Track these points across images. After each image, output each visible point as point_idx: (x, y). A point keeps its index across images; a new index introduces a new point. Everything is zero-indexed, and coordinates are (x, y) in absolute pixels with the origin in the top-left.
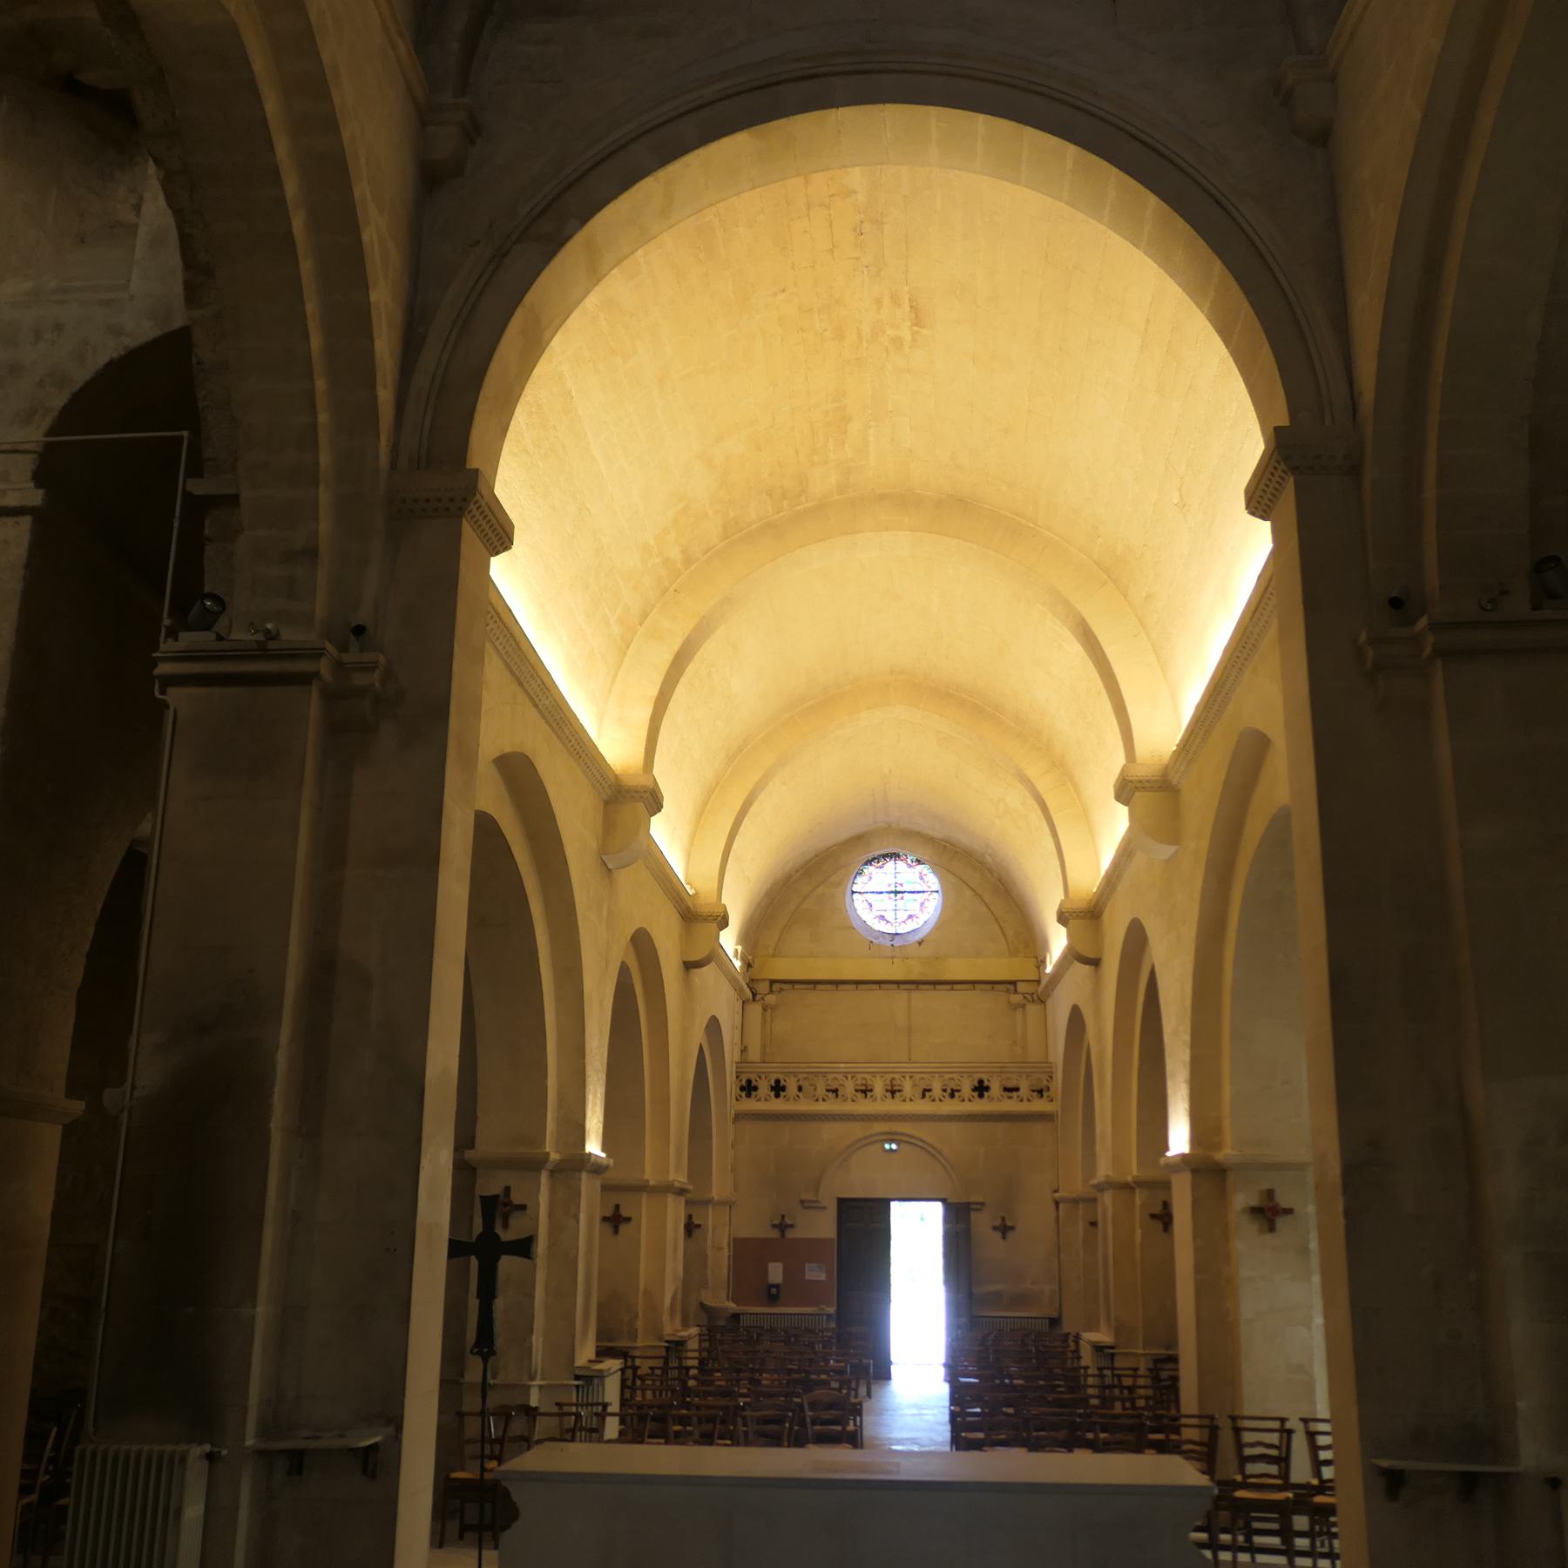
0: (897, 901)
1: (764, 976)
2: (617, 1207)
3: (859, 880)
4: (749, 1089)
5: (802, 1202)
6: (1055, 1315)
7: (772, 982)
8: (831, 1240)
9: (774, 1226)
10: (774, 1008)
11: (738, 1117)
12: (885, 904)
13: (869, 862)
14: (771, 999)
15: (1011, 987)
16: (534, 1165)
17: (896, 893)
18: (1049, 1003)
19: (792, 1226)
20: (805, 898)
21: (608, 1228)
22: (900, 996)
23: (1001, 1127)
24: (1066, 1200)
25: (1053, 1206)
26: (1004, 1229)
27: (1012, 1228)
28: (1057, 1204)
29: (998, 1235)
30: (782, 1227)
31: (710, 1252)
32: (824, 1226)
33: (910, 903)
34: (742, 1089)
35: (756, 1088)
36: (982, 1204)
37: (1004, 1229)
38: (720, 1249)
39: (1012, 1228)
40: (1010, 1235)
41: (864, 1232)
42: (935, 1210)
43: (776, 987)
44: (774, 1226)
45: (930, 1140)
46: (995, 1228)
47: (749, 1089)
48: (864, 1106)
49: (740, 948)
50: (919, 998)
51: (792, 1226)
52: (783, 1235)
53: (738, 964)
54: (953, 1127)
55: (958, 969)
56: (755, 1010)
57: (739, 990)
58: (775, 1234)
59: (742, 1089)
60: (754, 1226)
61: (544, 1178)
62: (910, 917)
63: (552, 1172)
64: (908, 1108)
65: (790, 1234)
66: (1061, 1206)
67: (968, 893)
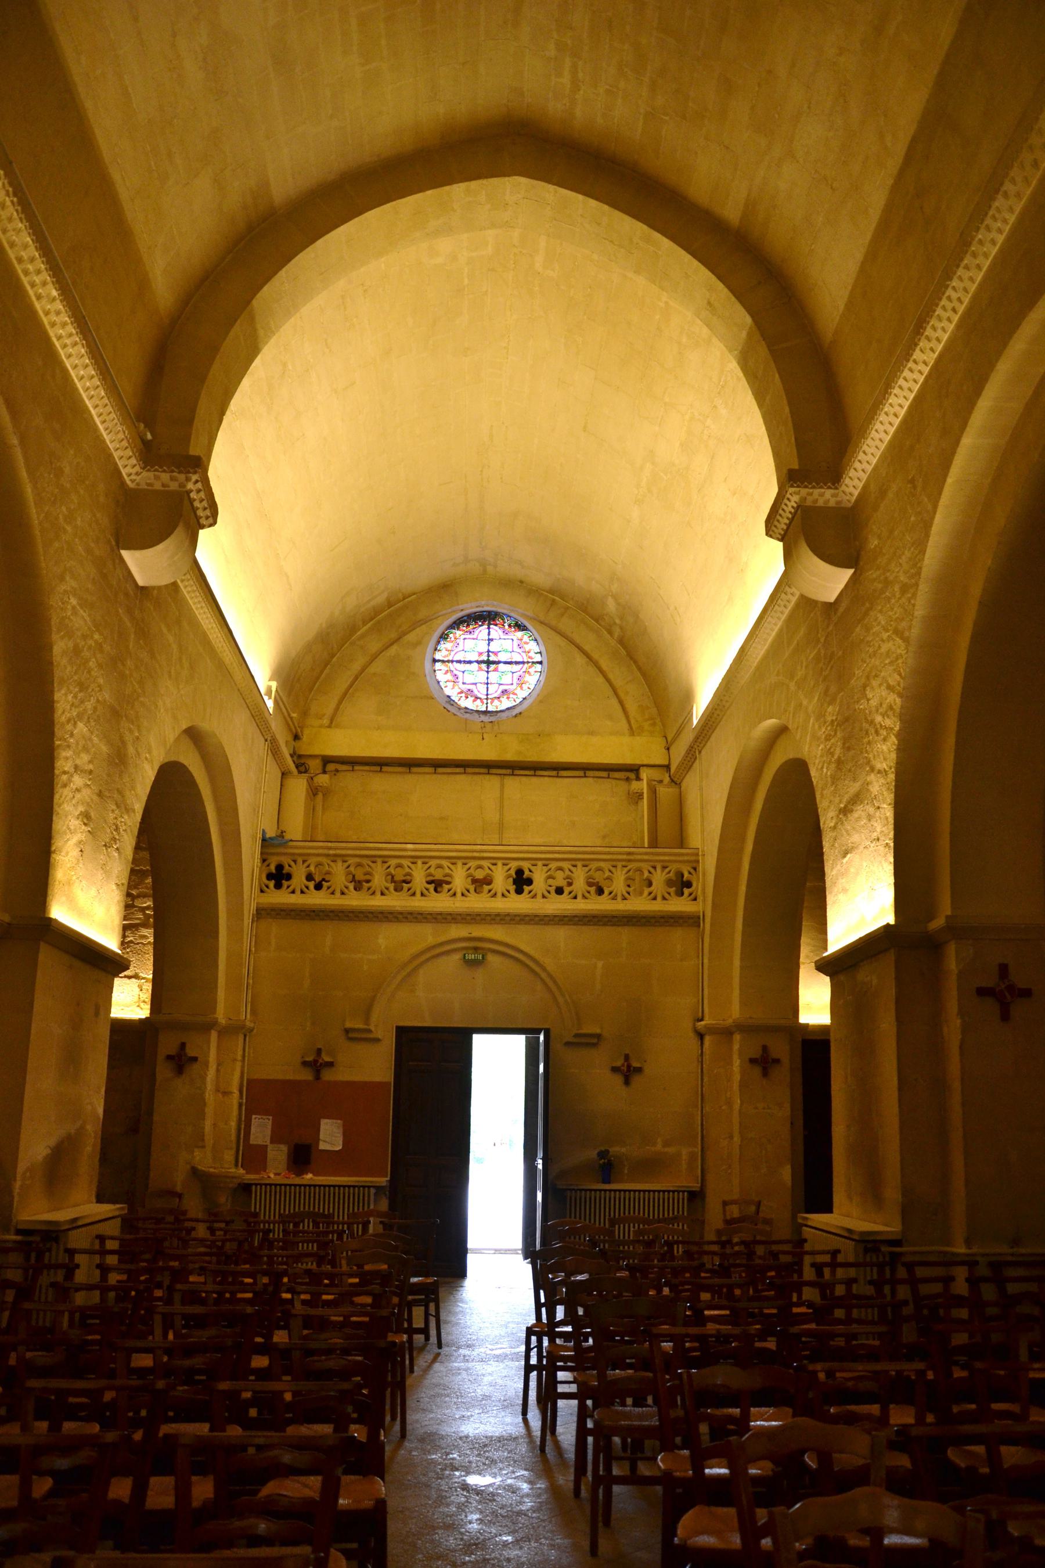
0: (488, 670)
1: (317, 752)
2: (183, 1045)
3: (444, 646)
4: (279, 877)
5: (347, 1031)
6: (696, 1186)
7: (327, 760)
8: (389, 1083)
9: (305, 1064)
10: (327, 792)
11: (262, 913)
12: (475, 675)
13: (456, 624)
14: (323, 780)
15: (632, 776)
16: (208, 1027)
17: (489, 663)
18: (684, 785)
19: (331, 1064)
20: (374, 657)
21: (757, 1071)
22: (490, 784)
23: (625, 935)
24: (712, 1030)
25: (695, 1042)
26: (628, 1072)
27: (639, 1070)
28: (701, 1036)
29: (619, 1079)
30: (317, 1066)
31: (210, 1096)
32: (374, 1065)
33: (503, 676)
34: (270, 876)
35: (289, 877)
36: (599, 1036)
37: (628, 1072)
38: (226, 1093)
39: (639, 1070)
40: (637, 1080)
41: (435, 1074)
42: (517, 1043)
43: (331, 767)
44: (305, 1064)
45: (532, 953)
46: (615, 1070)
47: (279, 877)
48: (440, 903)
49: (274, 685)
50: (515, 786)
51: (331, 1064)
52: (318, 1078)
53: (270, 704)
54: (560, 935)
55: (566, 749)
56: (299, 786)
57: (274, 750)
58: (307, 1075)
59: (270, 876)
60: (281, 1063)
61: (214, 1035)
62: (504, 692)
63: (219, 1032)
64: (500, 905)
65: (328, 1075)
66: (707, 1040)
67: (580, 660)
